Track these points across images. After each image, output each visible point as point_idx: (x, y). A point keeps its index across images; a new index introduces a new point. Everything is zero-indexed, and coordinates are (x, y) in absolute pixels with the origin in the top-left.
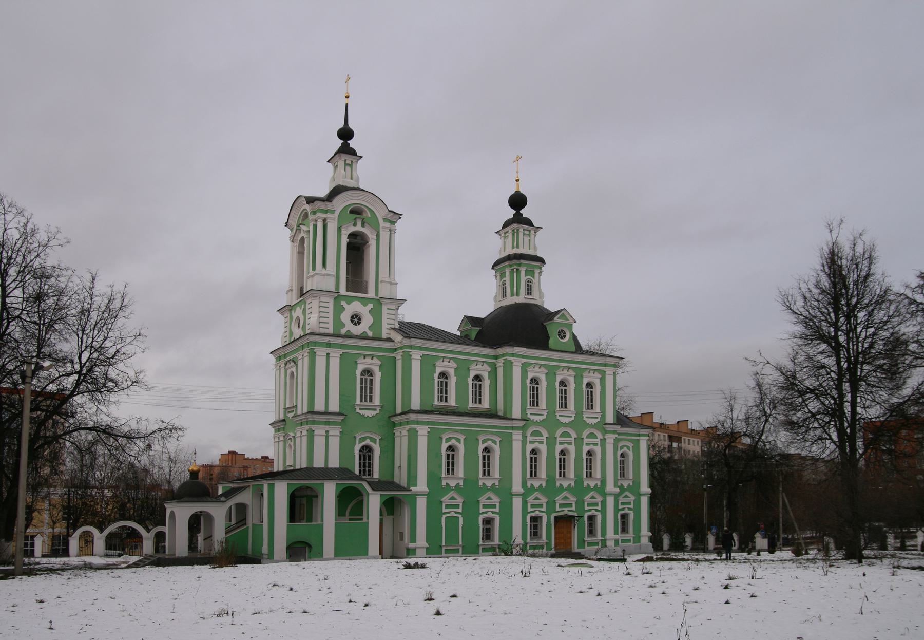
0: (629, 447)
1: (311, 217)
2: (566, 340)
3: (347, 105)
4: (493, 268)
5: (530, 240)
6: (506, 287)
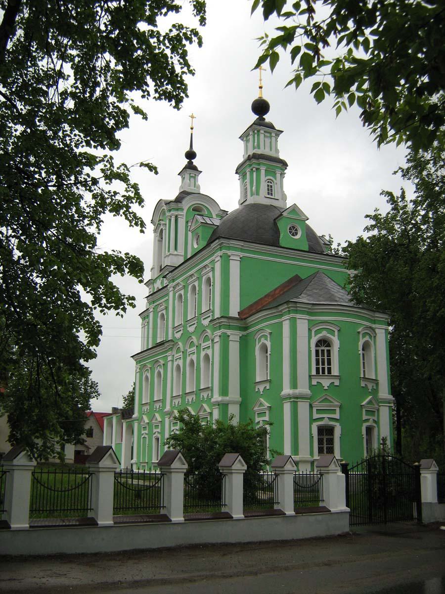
1: (168, 214)
3: (192, 134)
5: (271, 142)
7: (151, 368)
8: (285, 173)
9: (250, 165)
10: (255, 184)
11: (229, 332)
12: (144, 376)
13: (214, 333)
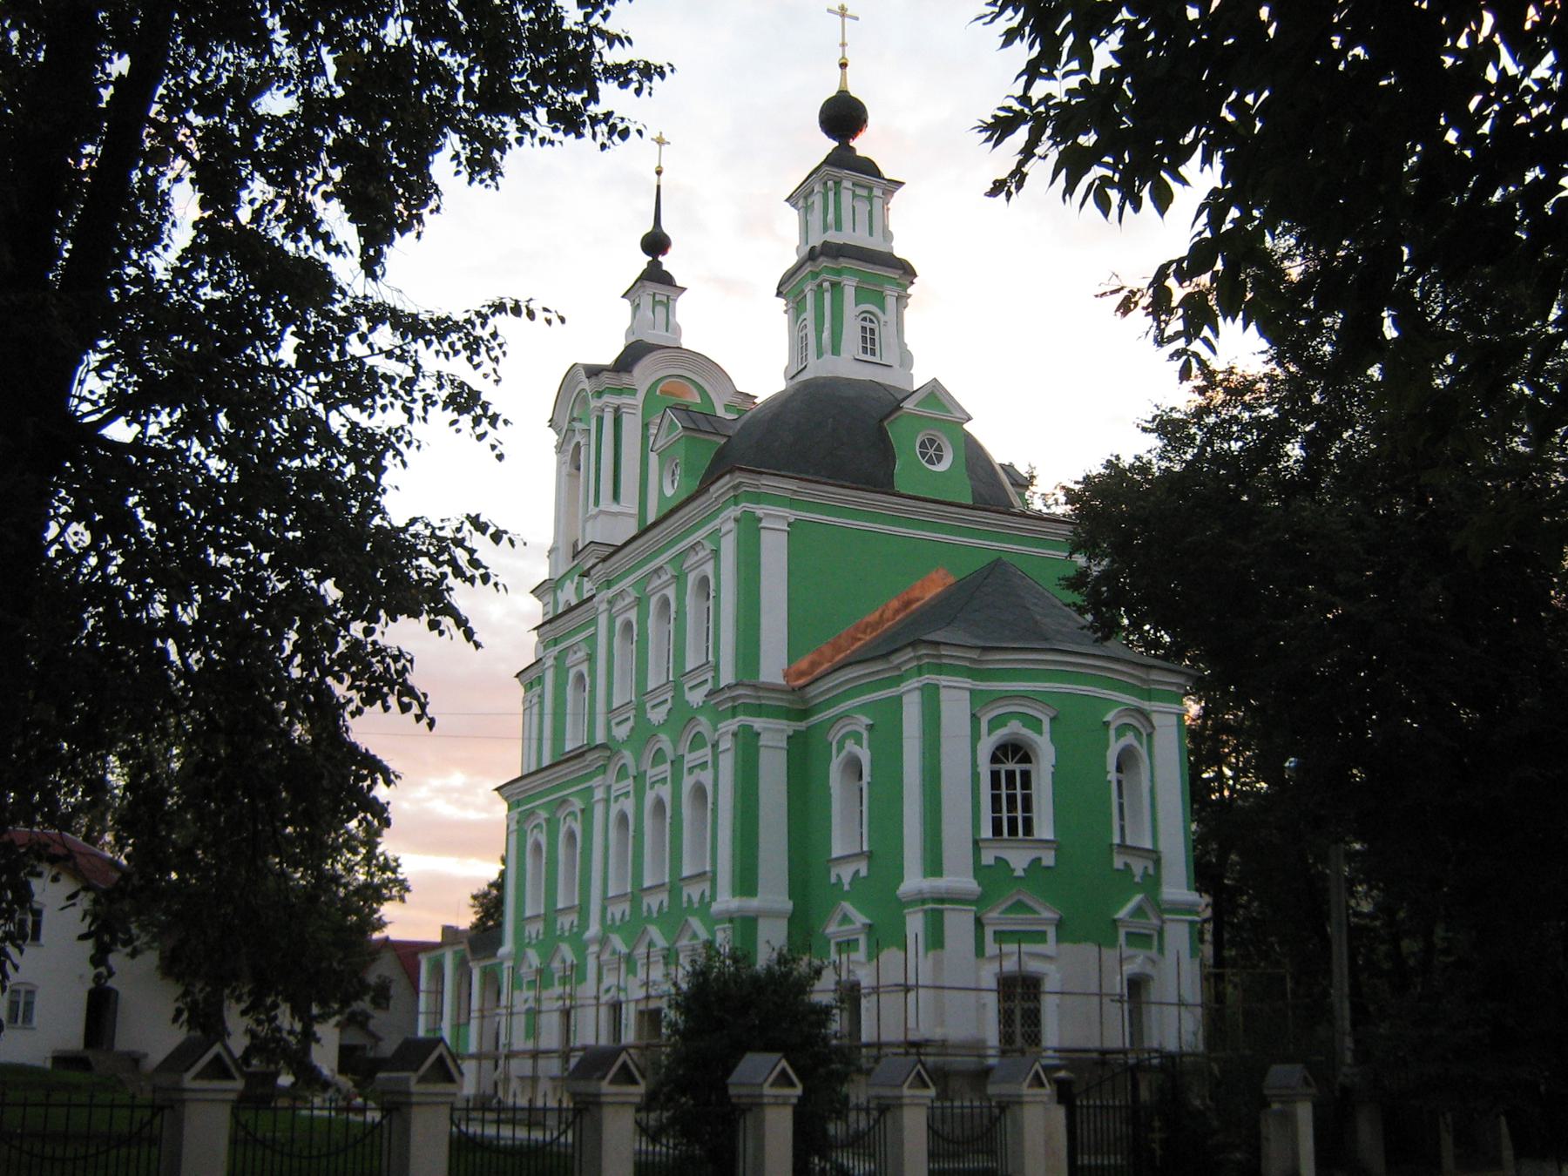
0: (1140, 733)
4: (779, 294)
8: (910, 296)
11: (758, 723)
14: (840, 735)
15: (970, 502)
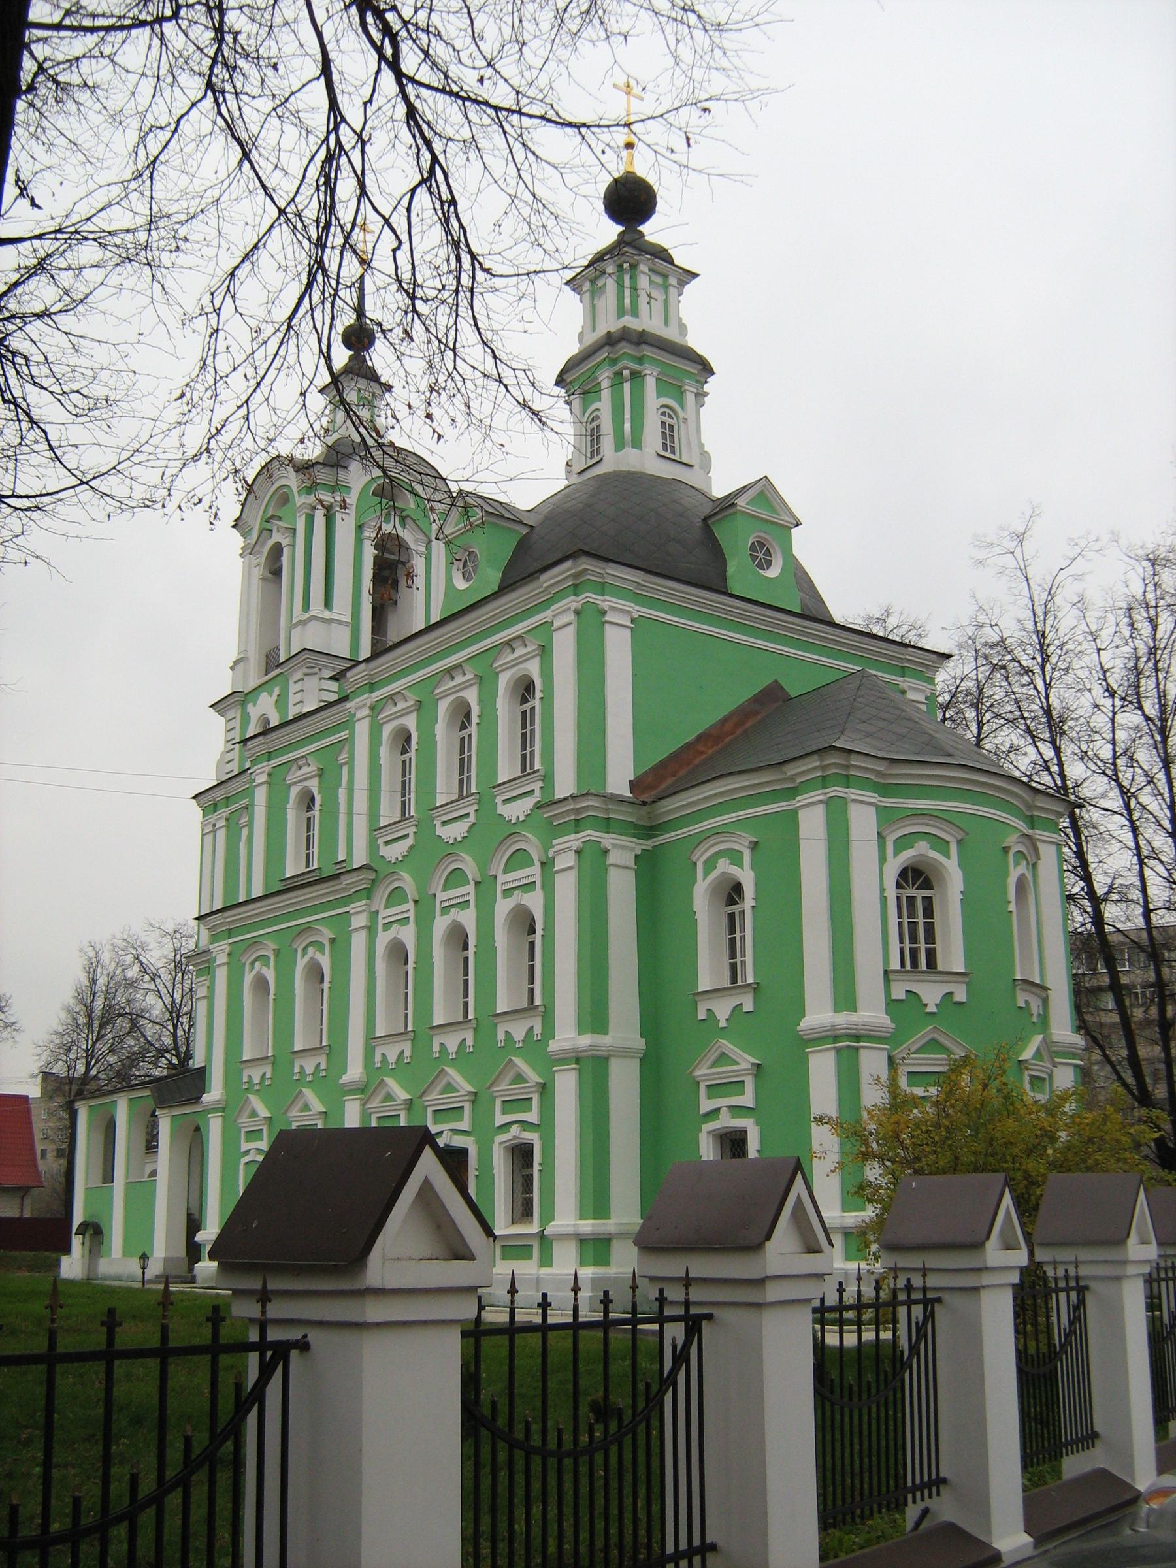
2: (773, 572)
6: (599, 426)
7: (277, 952)
8: (706, 394)
9: (614, 362)
10: (627, 416)
11: (607, 840)
12: (249, 978)
13: (555, 842)
14: (708, 854)
15: (799, 611)
